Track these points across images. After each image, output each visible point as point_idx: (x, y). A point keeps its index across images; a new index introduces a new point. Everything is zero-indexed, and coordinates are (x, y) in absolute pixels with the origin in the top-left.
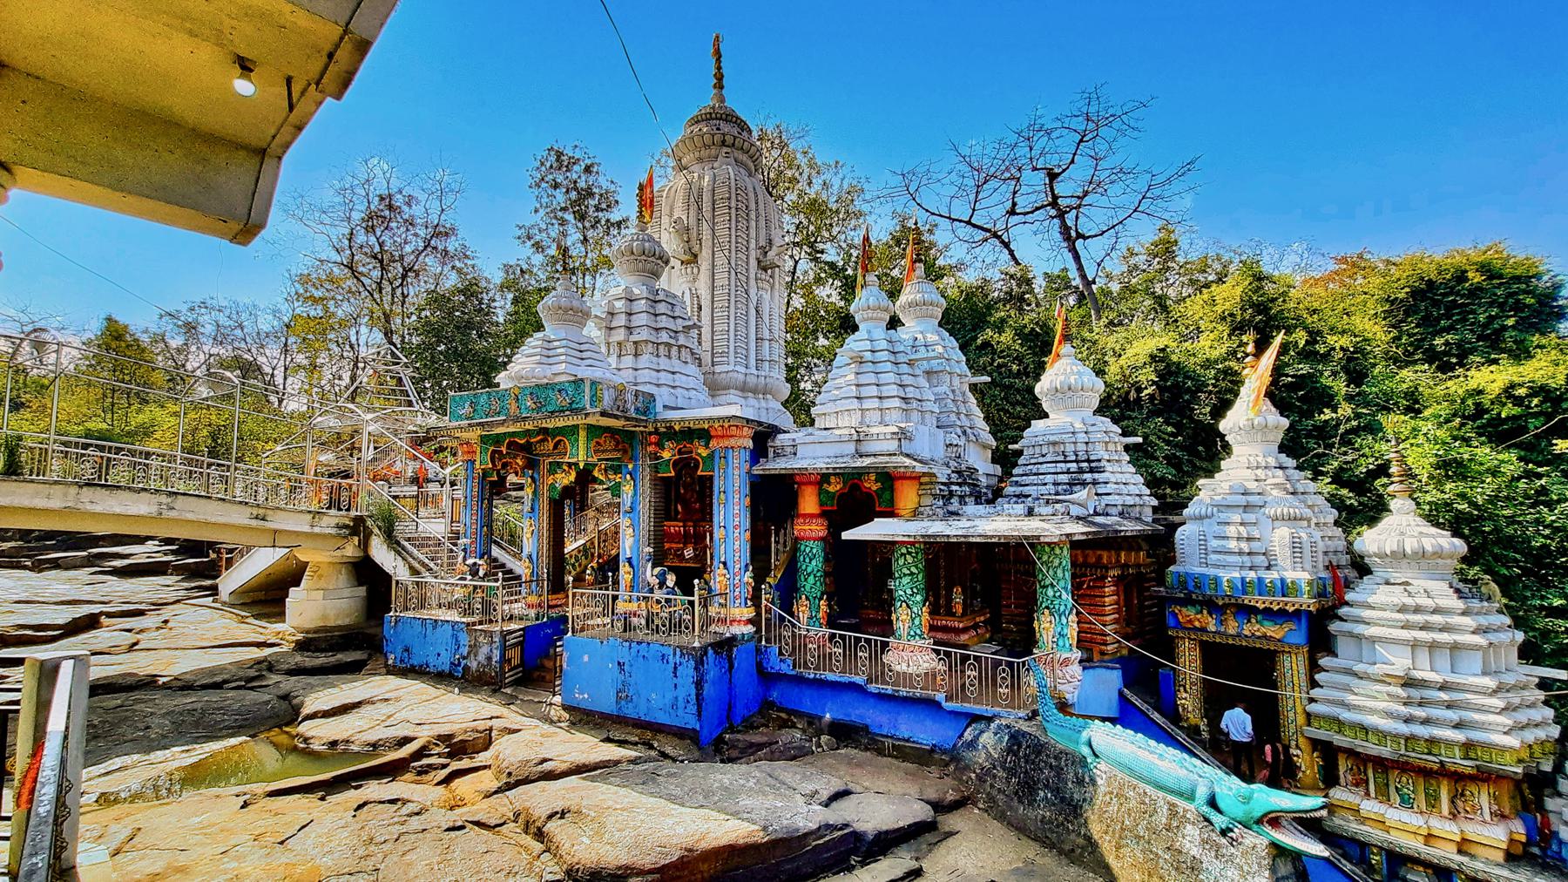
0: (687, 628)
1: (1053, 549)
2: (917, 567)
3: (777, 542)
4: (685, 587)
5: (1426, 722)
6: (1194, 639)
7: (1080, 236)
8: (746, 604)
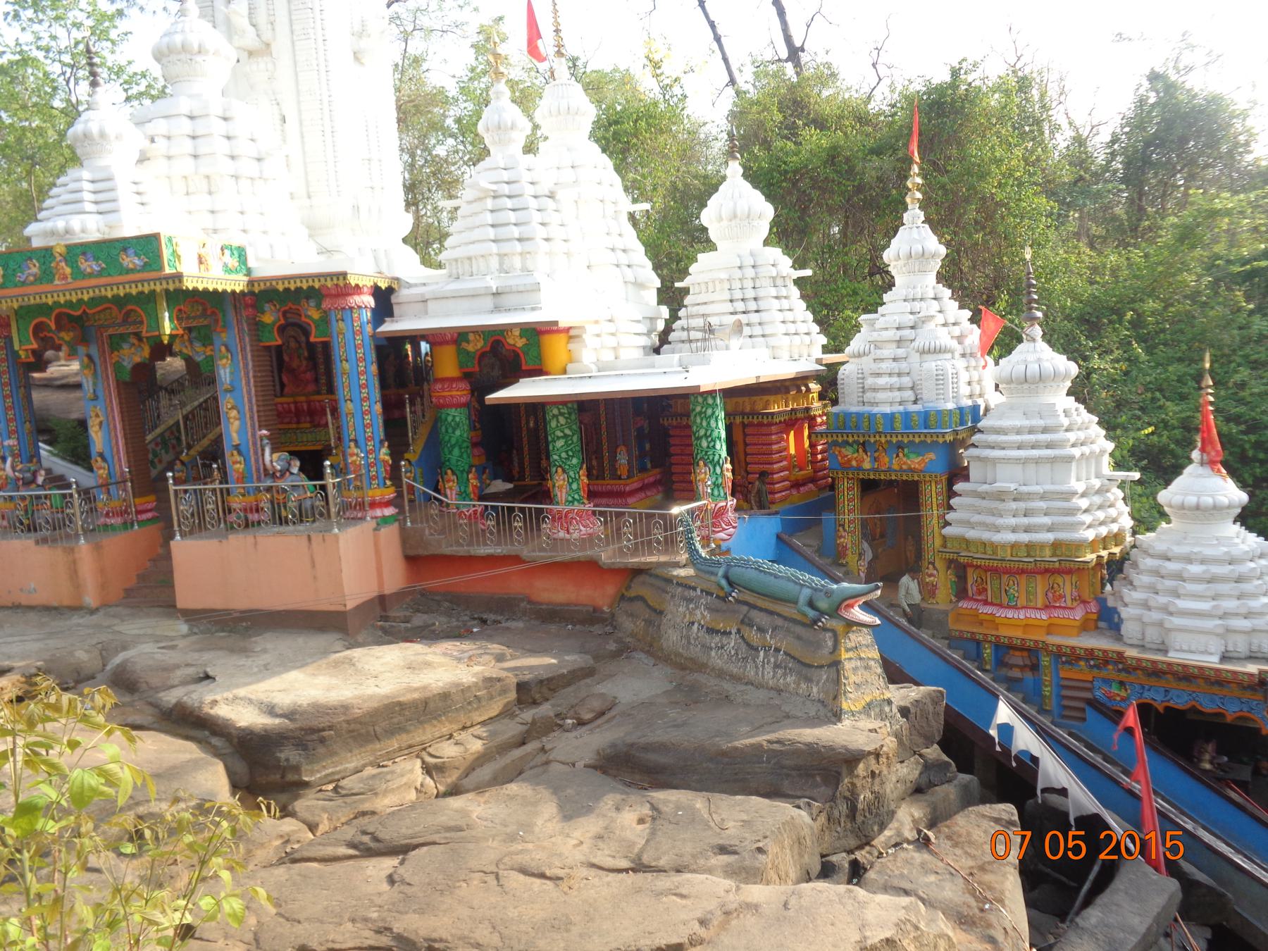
0: (321, 515)
1: (705, 399)
2: (570, 428)
4: (312, 466)
5: (1027, 530)
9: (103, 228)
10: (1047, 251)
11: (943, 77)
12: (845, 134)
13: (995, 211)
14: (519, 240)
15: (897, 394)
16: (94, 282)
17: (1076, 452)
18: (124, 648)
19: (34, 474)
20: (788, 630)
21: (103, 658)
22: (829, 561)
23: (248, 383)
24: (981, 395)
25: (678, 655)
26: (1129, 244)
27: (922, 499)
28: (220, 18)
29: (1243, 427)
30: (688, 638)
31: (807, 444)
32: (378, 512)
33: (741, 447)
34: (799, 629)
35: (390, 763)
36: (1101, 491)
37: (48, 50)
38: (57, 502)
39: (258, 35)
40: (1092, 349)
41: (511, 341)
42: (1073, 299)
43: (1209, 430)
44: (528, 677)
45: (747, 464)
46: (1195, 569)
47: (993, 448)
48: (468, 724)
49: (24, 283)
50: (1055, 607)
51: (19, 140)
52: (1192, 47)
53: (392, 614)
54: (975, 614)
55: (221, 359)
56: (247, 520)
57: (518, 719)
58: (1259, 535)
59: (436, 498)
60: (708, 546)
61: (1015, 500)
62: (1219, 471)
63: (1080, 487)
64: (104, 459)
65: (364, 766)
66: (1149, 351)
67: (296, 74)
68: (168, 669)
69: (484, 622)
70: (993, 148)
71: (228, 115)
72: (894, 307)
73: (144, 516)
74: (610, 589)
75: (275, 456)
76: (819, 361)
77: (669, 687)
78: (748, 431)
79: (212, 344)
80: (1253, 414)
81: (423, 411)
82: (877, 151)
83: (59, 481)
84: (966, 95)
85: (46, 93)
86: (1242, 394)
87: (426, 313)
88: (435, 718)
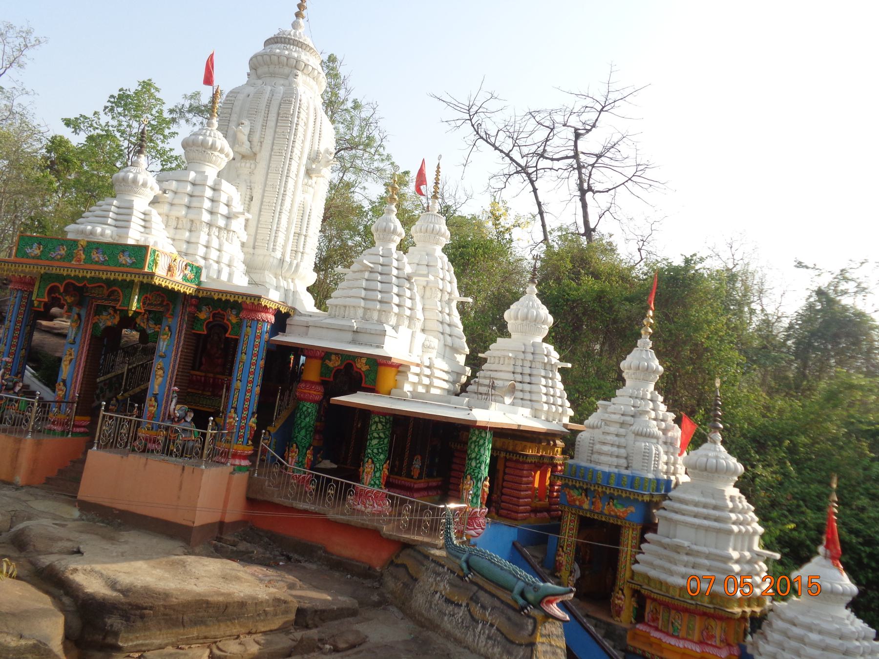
1: (480, 433)
2: (384, 433)
3: (281, 400)
4: (200, 421)
6: (575, 514)
7: (590, 189)
8: (248, 442)
9: (115, 236)
10: (735, 388)
11: (678, 262)
12: (611, 285)
13: (702, 354)
14: (380, 302)
15: (615, 459)
16: (97, 267)
17: (735, 528)
18: (29, 519)
19: (15, 384)
20: (502, 612)
21: (12, 522)
22: (547, 571)
23: (176, 355)
24: (674, 474)
25: (421, 614)
26: (792, 396)
27: (623, 539)
28: (230, 133)
29: (860, 540)
30: (431, 603)
31: (548, 483)
32: (237, 462)
33: (501, 474)
34: (510, 613)
35: (187, 647)
36: (751, 562)
37: (123, 132)
38: (23, 406)
39: (251, 148)
40: (759, 461)
41: (359, 366)
42: (749, 424)
43: (833, 533)
44: (307, 605)
45: (503, 487)
46: (814, 637)
47: (676, 512)
48: (254, 631)
49: (53, 259)
50: (707, 644)
51: (88, 180)
52: (846, 280)
53: (225, 537)
54: (647, 636)
55: (163, 335)
56: (145, 446)
57: (291, 636)
58: (865, 622)
59: (279, 461)
60: (461, 538)
61: (687, 554)
62: (838, 566)
63: (735, 555)
64: (65, 385)
65: (167, 645)
66: (799, 471)
67: (267, 174)
68: (53, 539)
69: (289, 559)
70: (706, 313)
71: (217, 187)
72: (622, 401)
73: (78, 430)
74: (385, 555)
75: (179, 406)
76: (565, 426)
77: (408, 637)
78: (508, 464)
79: (160, 324)
80: (869, 532)
81: (288, 400)
82: (630, 300)
83: (28, 392)
84: (693, 277)
85: (114, 156)
86: (862, 515)
87: (307, 334)
88: (230, 620)
